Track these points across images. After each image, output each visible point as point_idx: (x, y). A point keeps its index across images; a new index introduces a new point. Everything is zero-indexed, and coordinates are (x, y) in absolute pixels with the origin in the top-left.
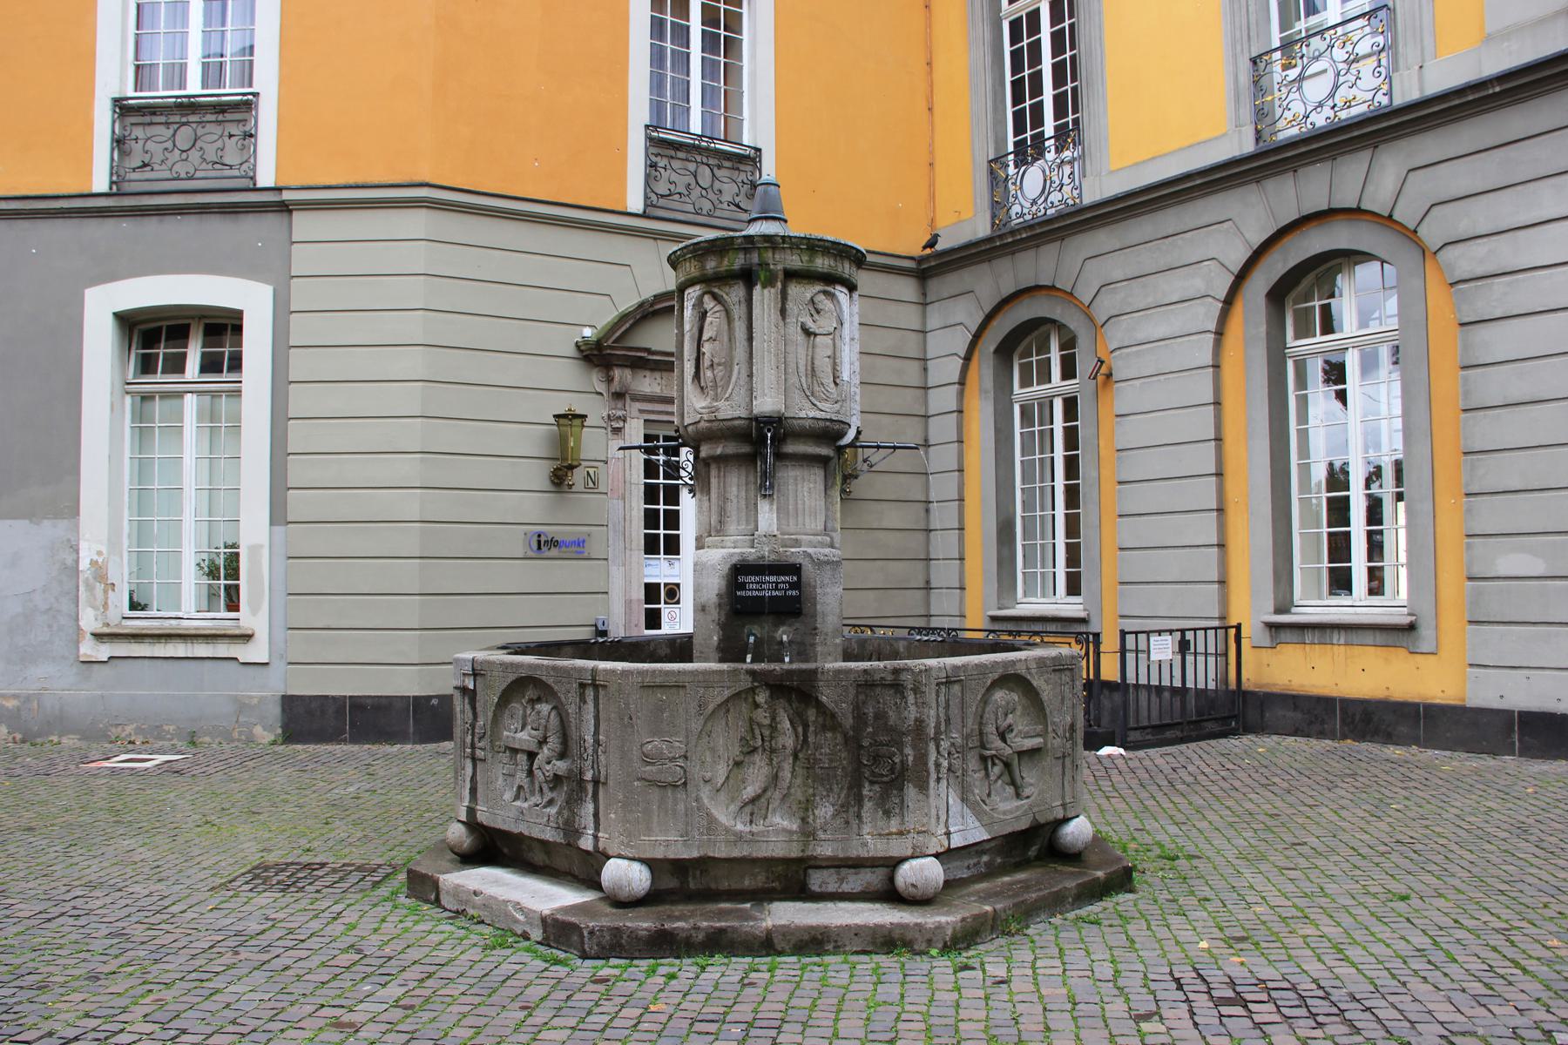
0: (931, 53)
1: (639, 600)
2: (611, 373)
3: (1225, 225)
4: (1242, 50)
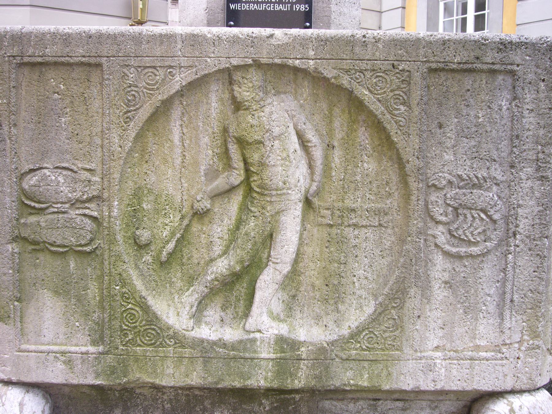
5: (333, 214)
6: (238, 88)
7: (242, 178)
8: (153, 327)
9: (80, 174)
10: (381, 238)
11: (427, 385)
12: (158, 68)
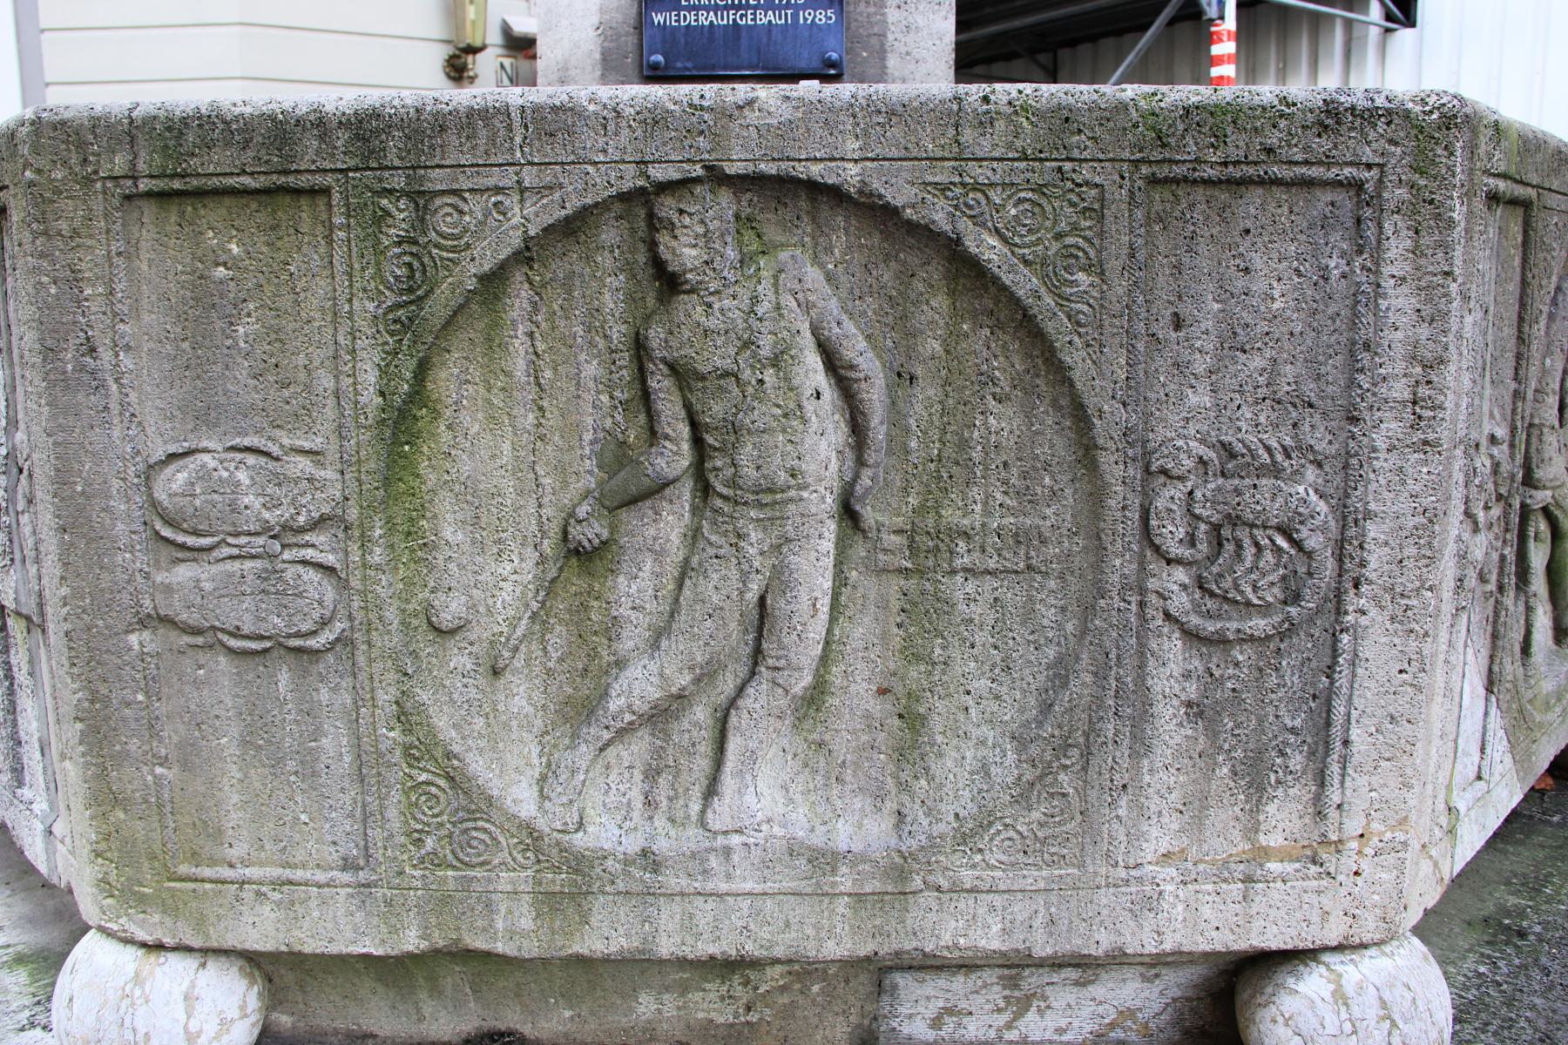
6: (667, 238)
8: (480, 824)
9: (288, 462)
10: (1031, 599)
12: (467, 195)
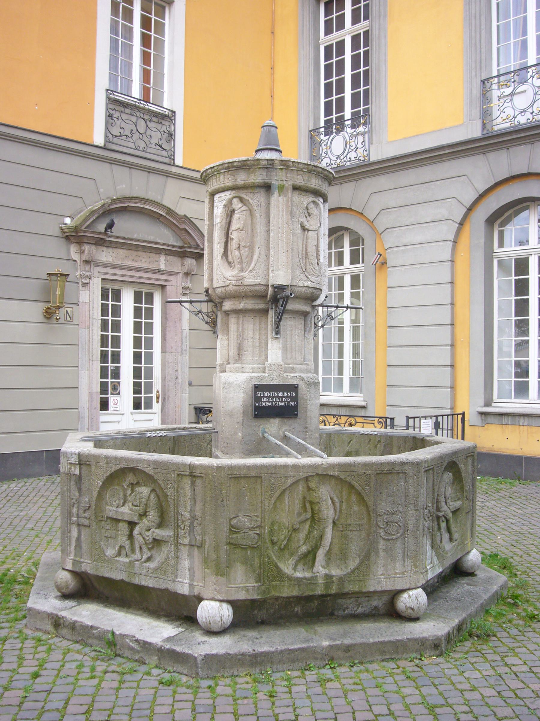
0: (274, 61)
1: (97, 392)
2: (83, 248)
3: (462, 178)
4: (476, 75)
5: (343, 527)
7: (311, 515)
11: (379, 589)
